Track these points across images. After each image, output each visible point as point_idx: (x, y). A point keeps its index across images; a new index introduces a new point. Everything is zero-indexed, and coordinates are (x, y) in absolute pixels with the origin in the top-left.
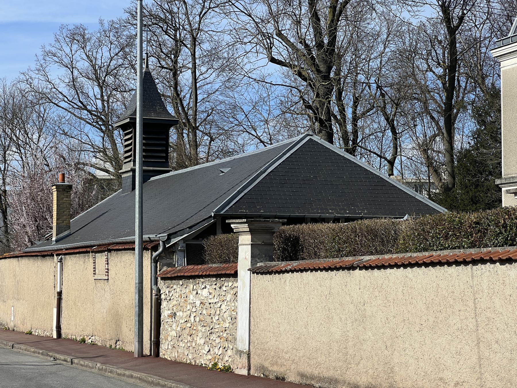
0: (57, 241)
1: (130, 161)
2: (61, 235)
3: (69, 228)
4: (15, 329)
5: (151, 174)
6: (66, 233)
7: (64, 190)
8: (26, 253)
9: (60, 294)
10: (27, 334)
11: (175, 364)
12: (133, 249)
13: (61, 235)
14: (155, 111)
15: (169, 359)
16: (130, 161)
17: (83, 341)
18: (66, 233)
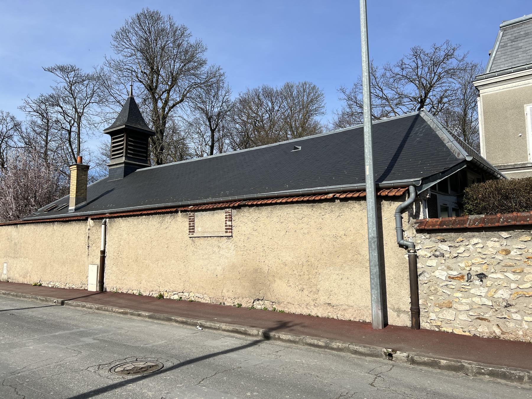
0: (76, 210)
1: (122, 156)
2: (80, 205)
3: (85, 199)
4: (10, 281)
5: (136, 167)
6: (83, 203)
7: (83, 169)
8: (24, 221)
9: (103, 252)
10: (35, 285)
11: (117, 295)
12: (364, 198)
13: (80, 205)
14: (140, 124)
15: (478, 335)
16: (122, 156)
17: (161, 296)
18: (83, 203)
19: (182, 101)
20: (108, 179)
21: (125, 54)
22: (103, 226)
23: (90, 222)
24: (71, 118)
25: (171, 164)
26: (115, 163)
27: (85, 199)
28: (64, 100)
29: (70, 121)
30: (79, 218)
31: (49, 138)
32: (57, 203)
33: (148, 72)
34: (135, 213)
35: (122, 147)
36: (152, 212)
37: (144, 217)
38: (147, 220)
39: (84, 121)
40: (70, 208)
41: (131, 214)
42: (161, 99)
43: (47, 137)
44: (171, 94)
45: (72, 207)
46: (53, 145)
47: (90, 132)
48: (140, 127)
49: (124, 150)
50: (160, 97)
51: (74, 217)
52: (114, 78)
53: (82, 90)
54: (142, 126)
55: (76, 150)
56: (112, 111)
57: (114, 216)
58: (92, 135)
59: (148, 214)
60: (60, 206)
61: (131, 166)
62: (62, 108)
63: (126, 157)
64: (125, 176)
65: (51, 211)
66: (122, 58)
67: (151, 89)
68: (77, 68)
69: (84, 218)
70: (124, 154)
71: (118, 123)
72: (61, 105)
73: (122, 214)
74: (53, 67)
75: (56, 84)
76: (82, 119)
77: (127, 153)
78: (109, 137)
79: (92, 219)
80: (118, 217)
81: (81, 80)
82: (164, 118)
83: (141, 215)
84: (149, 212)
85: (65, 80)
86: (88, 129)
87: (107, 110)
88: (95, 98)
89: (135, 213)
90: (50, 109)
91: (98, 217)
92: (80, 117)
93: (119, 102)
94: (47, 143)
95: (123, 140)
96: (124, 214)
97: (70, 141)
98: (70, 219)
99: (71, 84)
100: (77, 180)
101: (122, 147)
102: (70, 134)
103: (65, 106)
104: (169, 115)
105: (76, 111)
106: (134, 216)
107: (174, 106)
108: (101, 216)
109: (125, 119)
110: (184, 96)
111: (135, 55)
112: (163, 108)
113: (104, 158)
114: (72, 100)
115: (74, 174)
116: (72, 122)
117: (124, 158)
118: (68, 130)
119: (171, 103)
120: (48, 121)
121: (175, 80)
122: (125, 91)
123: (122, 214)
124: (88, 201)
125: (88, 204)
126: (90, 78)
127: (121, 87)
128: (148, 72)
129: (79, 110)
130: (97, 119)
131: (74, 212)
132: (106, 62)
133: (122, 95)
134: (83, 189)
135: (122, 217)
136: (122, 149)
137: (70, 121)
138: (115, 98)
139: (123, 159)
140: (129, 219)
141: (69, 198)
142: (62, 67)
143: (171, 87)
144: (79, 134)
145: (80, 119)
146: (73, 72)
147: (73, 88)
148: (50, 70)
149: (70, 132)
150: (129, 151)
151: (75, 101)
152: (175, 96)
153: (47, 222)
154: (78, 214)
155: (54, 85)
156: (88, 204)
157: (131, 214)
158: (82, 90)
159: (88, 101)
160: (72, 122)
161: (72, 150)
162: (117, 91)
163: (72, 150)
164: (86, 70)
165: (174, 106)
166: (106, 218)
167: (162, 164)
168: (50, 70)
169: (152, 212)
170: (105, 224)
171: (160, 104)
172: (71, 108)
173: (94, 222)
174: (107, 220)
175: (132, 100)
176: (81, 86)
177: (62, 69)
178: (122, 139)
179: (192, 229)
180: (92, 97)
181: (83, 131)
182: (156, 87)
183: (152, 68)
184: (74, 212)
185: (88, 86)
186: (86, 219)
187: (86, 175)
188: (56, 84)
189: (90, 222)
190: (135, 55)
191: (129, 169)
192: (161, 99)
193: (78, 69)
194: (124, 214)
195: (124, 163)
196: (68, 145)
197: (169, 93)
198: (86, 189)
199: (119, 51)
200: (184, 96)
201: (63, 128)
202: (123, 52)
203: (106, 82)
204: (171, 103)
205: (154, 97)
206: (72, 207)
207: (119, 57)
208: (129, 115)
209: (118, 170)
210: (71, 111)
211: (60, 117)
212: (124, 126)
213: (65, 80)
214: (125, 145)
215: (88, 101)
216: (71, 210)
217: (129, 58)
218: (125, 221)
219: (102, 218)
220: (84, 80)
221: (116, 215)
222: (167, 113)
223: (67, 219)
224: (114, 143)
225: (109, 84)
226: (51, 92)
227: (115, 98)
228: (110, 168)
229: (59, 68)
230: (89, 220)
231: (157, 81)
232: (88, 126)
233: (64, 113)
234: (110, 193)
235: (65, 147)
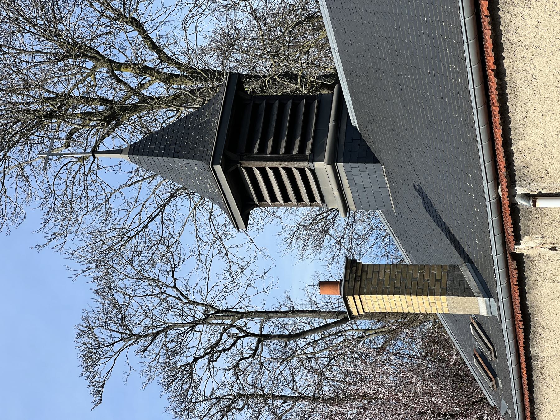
0: (488, 293)
1: (313, 171)
2: (473, 284)
3: (454, 268)
5: (344, 127)
6: (467, 274)
14: (208, 123)
16: (313, 171)
18: (467, 274)
19: (137, 25)
20: (387, 213)
21: (23, 196)
22: (540, 203)
23: (526, 246)
24: (225, 336)
25: (333, 44)
26: (337, 193)
27: (454, 268)
28: (176, 353)
29: (231, 336)
30: (515, 281)
31: (287, 392)
32: (468, 354)
33: (65, 128)
34: (494, 95)
35: (283, 173)
36: (488, 33)
37: (506, 63)
38: (520, 52)
39: (230, 302)
40: (484, 312)
41: (496, 109)
42: (141, 86)
43: (285, 398)
44: (121, 59)
45: (479, 306)
46: (304, 381)
47: (259, 284)
48: (216, 121)
49: (293, 165)
50: (135, 91)
51: (510, 297)
52: (91, 220)
53: (141, 308)
54: (213, 116)
55: (317, 322)
56: (190, 227)
57: (506, 171)
58: (268, 281)
59: (498, 48)
60: (478, 344)
61: (342, 141)
62: (196, 359)
63: (312, 159)
64: (375, 161)
65: (495, 367)
66: (34, 204)
67: (113, 116)
68: (82, 322)
69: (513, 265)
70: (305, 165)
71: (212, 187)
72: (191, 359)
73: (499, 142)
74: (87, 382)
75: (135, 375)
76: (222, 306)
77: (301, 157)
78: (255, 214)
79: (518, 239)
80: (509, 155)
81: (115, 312)
82: (194, 74)
83: (500, 73)
84: (489, 44)
85: (120, 351)
86: (250, 291)
87: (188, 240)
88: (160, 270)
89: (494, 95)
90: (206, 388)
91: (508, 221)
92: (219, 313)
93: (162, 208)
94: (302, 397)
95: (262, 170)
96: (498, 132)
97: (289, 337)
98: (518, 310)
99: (130, 337)
100: (394, 293)
101: (283, 173)
102: (267, 337)
103: (193, 351)
104: (183, 60)
105: (203, 321)
106: (503, 98)
107: (154, 47)
108: (507, 211)
109: (196, 165)
110: (120, 16)
111: (20, 166)
112: (169, 79)
113: (328, 242)
114: (172, 333)
115: (374, 303)
116: (234, 330)
117: (318, 166)
118: (259, 342)
119: (150, 59)
120: (239, 395)
121: (76, 50)
122: (130, 192)
123: (499, 142)
124: (457, 259)
125: (467, 259)
126: (106, 290)
127: (116, 201)
128: (65, 128)
129: (200, 315)
130: (219, 265)
131: (497, 300)
132: (53, 244)
133: (142, 199)
134: (422, 275)
135: (507, 143)
136: (289, 171)
137: (231, 336)
138: (152, 218)
139: (323, 168)
140: (516, 115)
141: (450, 317)
142: (86, 361)
143: (98, 57)
144: (268, 315)
145: (223, 311)
146: (96, 331)
147: (137, 331)
148: (98, 390)
149: (262, 338)
150: (295, 151)
151: (175, 325)
152: (123, 45)
153: (530, 376)
154: (500, 285)
155: (137, 379)
156: (467, 259)
157: (496, 109)
158: (141, 308)
159: (170, 291)
160: (234, 330)
161: (314, 330)
162: (132, 215)
163: (314, 330)
164: (83, 297)
165: (154, 47)
166: (512, 195)
167: (335, 76)
168: (98, 390)
169: (488, 33)
170: (532, 197)
171: (156, 89)
172: (197, 335)
173: (527, 233)
174: (519, 190)
175: (134, 150)
176: (130, 311)
177: (91, 358)
178: (257, 173)
179: (534, 205)
180: (157, 281)
181: (259, 303)
182: (102, 101)
183: (51, 115)
184: (497, 300)
185: (128, 291)
186: (519, 259)
187: (376, 268)
188: (135, 375)
189: (526, 246)
190: (20, 166)
191: (353, 149)
192: (141, 86)
193: (86, 319)
194: (498, 132)
195: (333, 162)
196: (301, 343)
197: (120, 66)
198: (422, 267)
199: (19, 212)
200: (120, 16)
201: (253, 355)
202: (19, 201)
203: (109, 244)
204: (150, 59)
205: (135, 108)
206: (479, 306)
207: (35, 214)
208: (183, 156)
209: (358, 180)
210: (206, 335)
211: (223, 362)
212: (218, 168)
213: (120, 351)
214: (276, 164)
215: (170, 291)
216: (489, 309)
217: (33, 183)
218: (523, 130)
219: (514, 209)
220: (115, 304)
221: (502, 162)
222: (179, 65)
223: (519, 317)
224: (274, 199)
225: (114, 233)
226: (156, 386)
227: (152, 218)
228: (352, 207)
229: (89, 368)
230: (519, 249)
231: (87, 100)
232: (241, 291)
233: (212, 352)
234: (431, 196)
235: (310, 350)
